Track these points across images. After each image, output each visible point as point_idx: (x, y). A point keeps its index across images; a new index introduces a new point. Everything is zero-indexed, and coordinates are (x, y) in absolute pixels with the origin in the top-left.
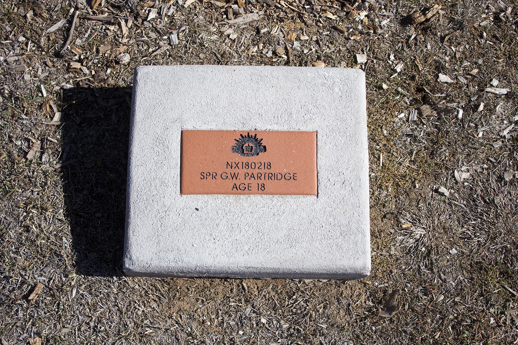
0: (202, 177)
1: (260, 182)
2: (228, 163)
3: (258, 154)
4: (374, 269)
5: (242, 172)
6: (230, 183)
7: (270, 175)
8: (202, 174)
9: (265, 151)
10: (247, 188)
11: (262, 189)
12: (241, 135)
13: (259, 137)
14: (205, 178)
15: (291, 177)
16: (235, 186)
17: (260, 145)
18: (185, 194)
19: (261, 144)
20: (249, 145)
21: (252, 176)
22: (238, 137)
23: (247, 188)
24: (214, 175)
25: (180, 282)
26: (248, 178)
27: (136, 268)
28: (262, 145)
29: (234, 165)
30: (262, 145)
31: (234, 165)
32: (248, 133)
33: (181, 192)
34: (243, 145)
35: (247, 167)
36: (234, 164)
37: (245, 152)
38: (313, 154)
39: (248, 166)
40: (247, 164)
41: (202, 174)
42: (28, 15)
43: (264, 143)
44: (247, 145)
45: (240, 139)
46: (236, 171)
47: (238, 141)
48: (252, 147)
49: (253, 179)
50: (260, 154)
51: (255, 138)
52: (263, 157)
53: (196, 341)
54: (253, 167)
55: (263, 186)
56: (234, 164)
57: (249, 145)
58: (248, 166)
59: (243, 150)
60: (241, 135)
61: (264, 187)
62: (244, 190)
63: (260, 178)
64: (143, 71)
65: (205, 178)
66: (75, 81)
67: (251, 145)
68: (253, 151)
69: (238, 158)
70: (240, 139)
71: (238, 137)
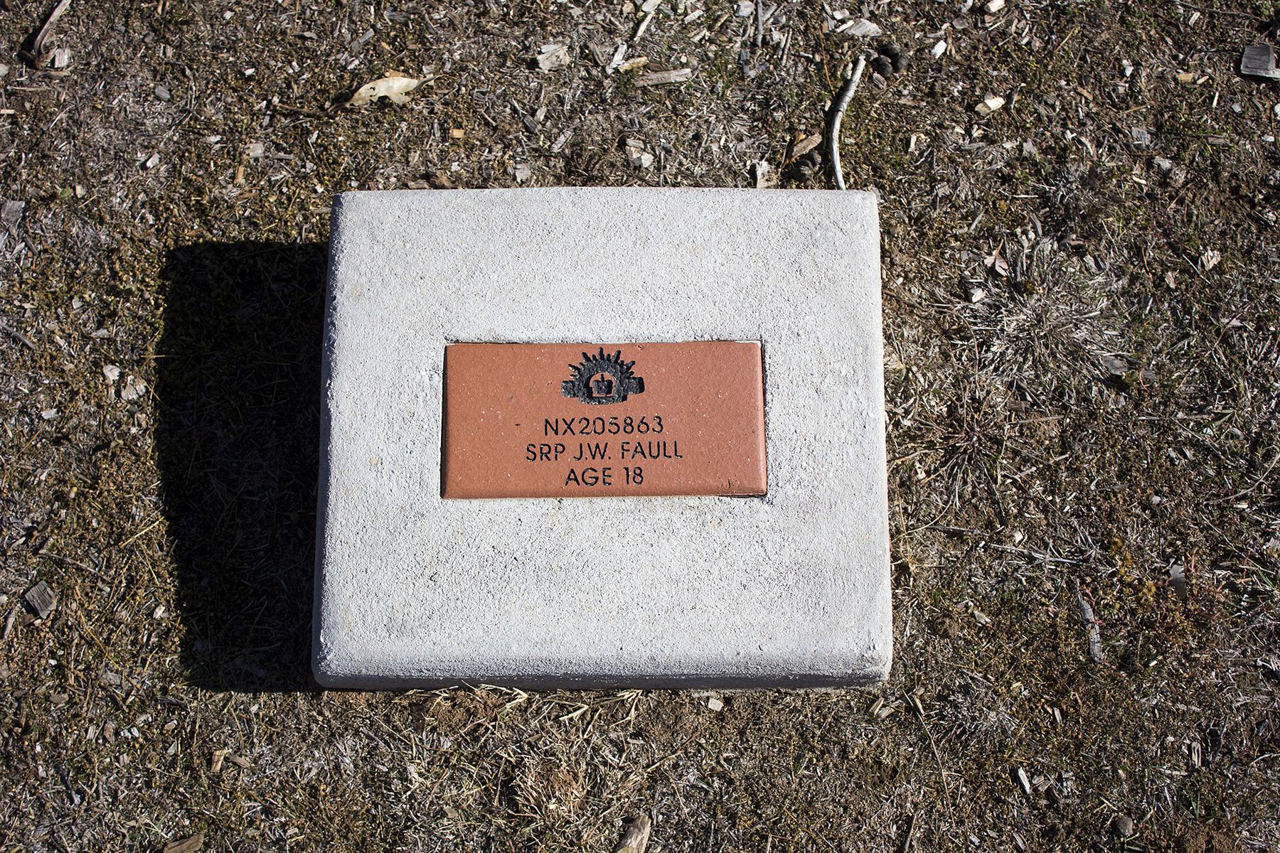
0: (532, 456)
2: (547, 421)
3: (625, 398)
4: (904, 651)
5: (614, 442)
7: (546, 450)
8: (531, 448)
9: (642, 389)
10: (600, 480)
12: (585, 355)
14: (538, 457)
15: (597, 479)
16: (572, 476)
18: (456, 497)
19: (633, 373)
20: (603, 378)
21: (639, 449)
22: (578, 361)
23: (600, 480)
25: (360, 701)
26: (628, 455)
29: (562, 427)
31: (562, 427)
32: (602, 349)
33: (443, 494)
34: (590, 378)
35: (643, 428)
36: (561, 423)
37: (595, 394)
39: (631, 425)
40: (628, 421)
41: (531, 448)
42: (162, 169)
43: (637, 372)
44: (598, 377)
45: (581, 364)
46: (602, 440)
49: (639, 456)
50: (631, 396)
51: (616, 362)
52: (635, 406)
54: (599, 429)
55: (639, 473)
56: (561, 423)
57: (603, 378)
60: (585, 355)
61: (640, 475)
66: (846, 180)
67: (608, 376)
68: (614, 389)
69: (579, 408)
70: (581, 364)
71: (578, 361)
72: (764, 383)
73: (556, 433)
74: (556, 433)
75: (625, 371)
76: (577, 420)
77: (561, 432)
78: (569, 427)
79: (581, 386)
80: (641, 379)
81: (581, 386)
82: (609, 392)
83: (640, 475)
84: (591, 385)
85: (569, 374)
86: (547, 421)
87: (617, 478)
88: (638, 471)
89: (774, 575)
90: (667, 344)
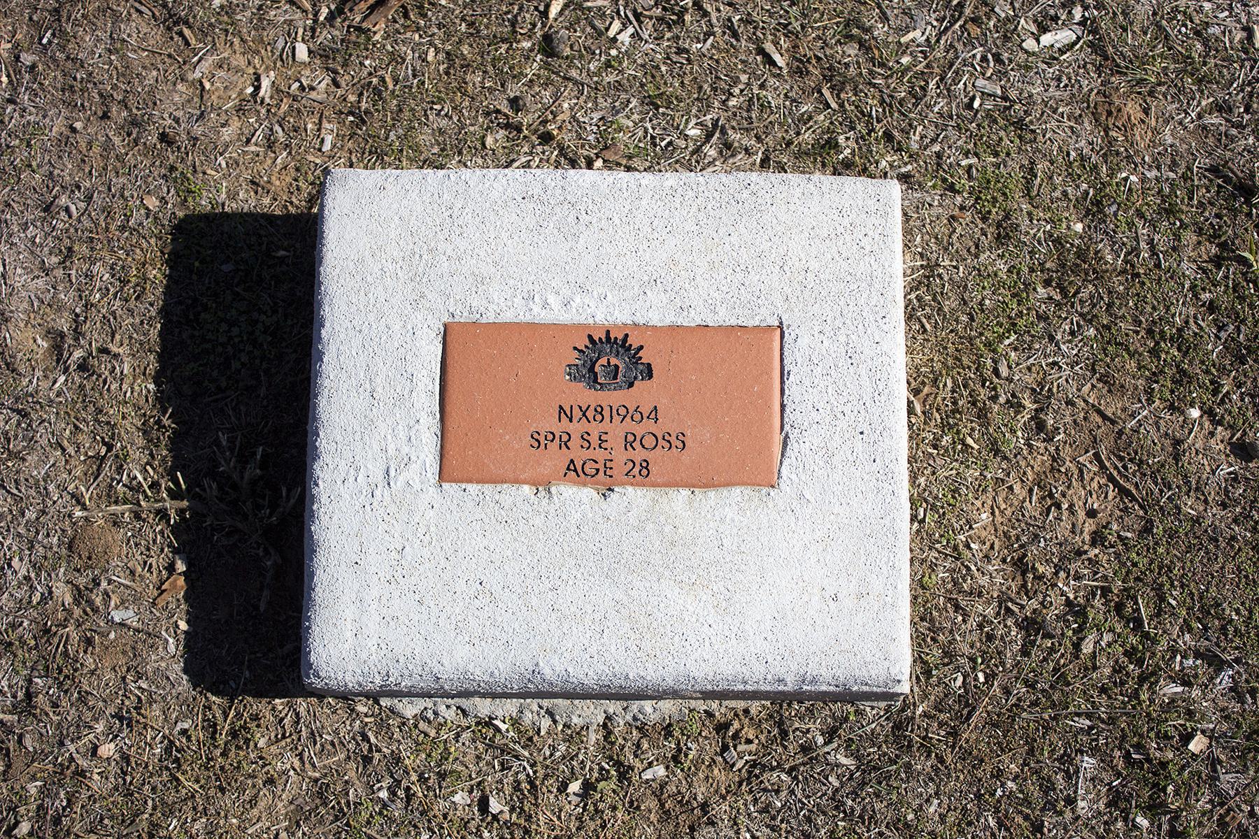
0: (536, 444)
1: (639, 455)
2: (561, 407)
3: (631, 385)
4: (923, 669)
5: (616, 431)
6: (555, 458)
8: (536, 436)
9: (650, 376)
10: (601, 473)
11: (642, 473)
12: (590, 337)
13: (634, 341)
14: (542, 446)
15: (598, 470)
17: (636, 363)
19: (640, 358)
20: (609, 362)
23: (601, 473)
24: (565, 438)
27: (318, 683)
28: (642, 361)
29: (577, 413)
30: (642, 361)
31: (577, 413)
32: (608, 332)
33: (443, 476)
35: (599, 417)
38: (769, 374)
39: (601, 413)
40: (599, 409)
41: (536, 436)
44: (603, 361)
45: (586, 347)
47: (581, 351)
48: (617, 367)
51: (623, 346)
52: (642, 394)
53: (1078, 13)
55: (646, 465)
57: (609, 362)
58: (601, 413)
59: (596, 374)
60: (590, 337)
62: (593, 476)
63: (566, 444)
64: (338, 172)
65: (542, 446)
67: (614, 361)
69: (583, 395)
71: (582, 343)
72: (782, 382)
73: (571, 421)
74: (571, 421)
75: (635, 359)
76: (592, 408)
77: (575, 420)
78: (584, 415)
79: (587, 373)
80: (649, 365)
81: (587, 373)
82: (615, 377)
83: (646, 468)
84: (597, 368)
85: (573, 357)
86: (561, 407)
87: (619, 468)
88: (644, 464)
89: (67, 742)
90: (654, 327)
